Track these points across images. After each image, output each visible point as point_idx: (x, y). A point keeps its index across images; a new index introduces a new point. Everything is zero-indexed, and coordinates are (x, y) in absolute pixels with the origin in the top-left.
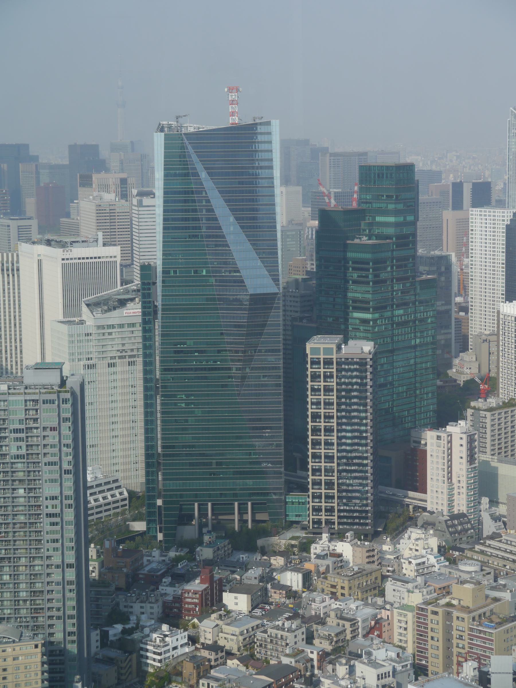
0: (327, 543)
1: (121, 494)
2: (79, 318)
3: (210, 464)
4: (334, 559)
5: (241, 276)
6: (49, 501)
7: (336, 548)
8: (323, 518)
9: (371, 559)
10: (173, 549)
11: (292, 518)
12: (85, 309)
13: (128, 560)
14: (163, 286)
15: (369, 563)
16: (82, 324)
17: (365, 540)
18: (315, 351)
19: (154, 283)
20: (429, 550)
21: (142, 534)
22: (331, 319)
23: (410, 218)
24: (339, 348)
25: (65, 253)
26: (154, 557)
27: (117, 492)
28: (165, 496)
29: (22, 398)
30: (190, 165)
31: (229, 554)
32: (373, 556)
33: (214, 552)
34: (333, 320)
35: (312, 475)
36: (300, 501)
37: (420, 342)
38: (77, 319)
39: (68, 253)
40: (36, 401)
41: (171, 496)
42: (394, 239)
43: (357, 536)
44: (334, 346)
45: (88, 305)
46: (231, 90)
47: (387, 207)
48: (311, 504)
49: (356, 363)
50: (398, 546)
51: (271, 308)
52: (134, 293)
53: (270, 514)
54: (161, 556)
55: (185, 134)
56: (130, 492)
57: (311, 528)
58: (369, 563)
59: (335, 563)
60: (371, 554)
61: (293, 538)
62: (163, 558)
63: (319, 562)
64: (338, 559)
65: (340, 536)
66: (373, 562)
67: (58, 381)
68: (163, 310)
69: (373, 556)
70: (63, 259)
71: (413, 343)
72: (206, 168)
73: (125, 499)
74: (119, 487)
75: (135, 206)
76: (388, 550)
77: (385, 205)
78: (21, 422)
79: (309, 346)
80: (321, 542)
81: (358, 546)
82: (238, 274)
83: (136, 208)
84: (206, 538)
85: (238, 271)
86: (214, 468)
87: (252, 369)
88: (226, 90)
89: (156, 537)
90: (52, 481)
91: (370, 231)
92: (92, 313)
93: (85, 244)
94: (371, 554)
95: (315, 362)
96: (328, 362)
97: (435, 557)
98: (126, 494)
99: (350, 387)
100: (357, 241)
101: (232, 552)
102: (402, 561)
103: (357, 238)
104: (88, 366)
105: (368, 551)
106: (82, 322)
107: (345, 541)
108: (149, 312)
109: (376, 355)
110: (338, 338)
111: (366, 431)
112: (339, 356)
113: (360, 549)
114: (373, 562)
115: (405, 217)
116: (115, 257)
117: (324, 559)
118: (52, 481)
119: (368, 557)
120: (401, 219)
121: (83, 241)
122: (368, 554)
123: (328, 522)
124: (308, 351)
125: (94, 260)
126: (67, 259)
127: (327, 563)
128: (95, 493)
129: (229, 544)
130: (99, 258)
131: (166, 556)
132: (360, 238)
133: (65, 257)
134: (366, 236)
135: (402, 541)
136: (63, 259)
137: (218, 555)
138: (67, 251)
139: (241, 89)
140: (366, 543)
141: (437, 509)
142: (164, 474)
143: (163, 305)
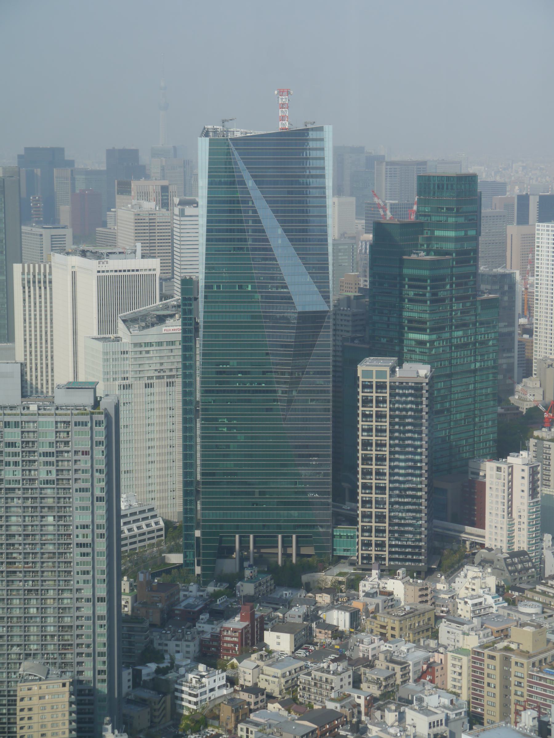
0: (377, 580)
1: (157, 523)
2: (115, 335)
3: (253, 493)
4: (384, 597)
6: (79, 529)
7: (386, 586)
8: (373, 553)
9: (424, 599)
10: (212, 583)
12: (121, 325)
14: (205, 302)
15: (421, 602)
16: (118, 341)
17: (418, 578)
18: (367, 374)
19: (196, 299)
20: (486, 590)
21: (179, 567)
23: (472, 233)
25: (101, 265)
27: (152, 522)
28: (204, 527)
29: (52, 419)
31: (271, 590)
32: (427, 595)
33: (256, 588)
34: (387, 341)
35: (362, 507)
38: (112, 336)
39: (104, 265)
40: (67, 423)
41: (210, 527)
42: (454, 255)
43: (410, 573)
44: (388, 369)
45: (124, 321)
46: (281, 92)
47: (447, 221)
49: (411, 388)
50: (453, 584)
51: (321, 327)
52: (174, 309)
53: (316, 548)
54: (199, 590)
55: (231, 139)
56: (167, 522)
58: (421, 602)
60: (424, 592)
62: (201, 593)
63: (368, 600)
64: (389, 598)
65: (391, 573)
67: (92, 402)
70: (99, 272)
71: (473, 367)
72: (253, 176)
73: (161, 530)
74: (155, 516)
75: (177, 215)
76: (442, 588)
77: (445, 218)
78: (51, 444)
80: (370, 579)
81: (411, 584)
82: (285, 290)
83: (178, 218)
84: (248, 573)
85: (286, 287)
87: (299, 392)
88: (276, 92)
90: (83, 508)
92: (129, 330)
94: (424, 592)
95: (367, 386)
96: (381, 386)
98: (162, 524)
99: (404, 413)
100: (414, 257)
101: (275, 588)
103: (414, 253)
104: (124, 386)
105: (421, 590)
109: (432, 379)
112: (394, 379)
113: (412, 587)
115: (466, 232)
116: (154, 270)
117: (373, 597)
118: (83, 508)
119: (421, 596)
120: (462, 233)
122: (420, 593)
123: (378, 558)
124: (359, 374)
126: (103, 272)
129: (271, 579)
130: (137, 270)
131: (203, 591)
132: (417, 254)
134: (424, 251)
135: (457, 579)
136: (99, 272)
137: (259, 591)
138: (103, 263)
139: (292, 92)
140: (419, 581)
142: (203, 503)
143: (204, 322)
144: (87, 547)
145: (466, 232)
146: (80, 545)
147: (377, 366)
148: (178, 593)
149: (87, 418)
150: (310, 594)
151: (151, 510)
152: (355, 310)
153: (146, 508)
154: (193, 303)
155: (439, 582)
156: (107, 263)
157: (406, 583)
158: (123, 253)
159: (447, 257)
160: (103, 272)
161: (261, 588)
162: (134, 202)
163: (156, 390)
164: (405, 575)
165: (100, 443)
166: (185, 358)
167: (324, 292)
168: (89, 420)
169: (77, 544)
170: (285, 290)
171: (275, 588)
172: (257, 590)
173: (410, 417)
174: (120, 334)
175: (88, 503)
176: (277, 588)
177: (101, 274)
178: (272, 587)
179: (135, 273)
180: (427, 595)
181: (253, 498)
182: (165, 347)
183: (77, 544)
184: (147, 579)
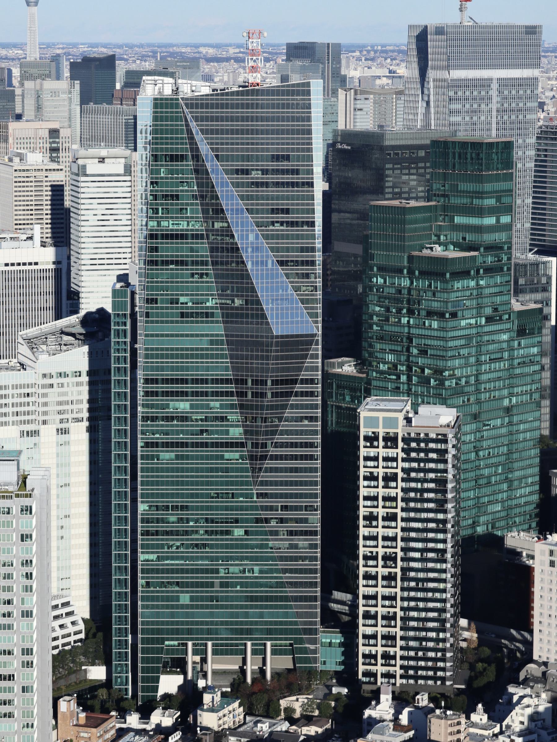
3: (212, 585)
18: (373, 422)
20: (539, 723)
23: (505, 219)
27: (67, 621)
37: (517, 402)
47: (472, 203)
51: (305, 357)
55: (182, 99)
71: (506, 402)
76: (479, 721)
77: (469, 200)
79: (364, 414)
86: (217, 592)
87: (276, 445)
96: (391, 441)
97: (549, 734)
99: (422, 475)
100: (426, 252)
103: (427, 248)
104: (28, 432)
109: (457, 425)
128: (76, 633)
129: (240, 707)
132: (431, 249)
139: (266, 34)
141: (540, 657)
145: (498, 220)
150: (294, 727)
153: (59, 602)
161: (226, 719)
165: (27, 537)
173: (432, 481)
180: (459, 732)
181: (212, 592)
184: (72, 709)
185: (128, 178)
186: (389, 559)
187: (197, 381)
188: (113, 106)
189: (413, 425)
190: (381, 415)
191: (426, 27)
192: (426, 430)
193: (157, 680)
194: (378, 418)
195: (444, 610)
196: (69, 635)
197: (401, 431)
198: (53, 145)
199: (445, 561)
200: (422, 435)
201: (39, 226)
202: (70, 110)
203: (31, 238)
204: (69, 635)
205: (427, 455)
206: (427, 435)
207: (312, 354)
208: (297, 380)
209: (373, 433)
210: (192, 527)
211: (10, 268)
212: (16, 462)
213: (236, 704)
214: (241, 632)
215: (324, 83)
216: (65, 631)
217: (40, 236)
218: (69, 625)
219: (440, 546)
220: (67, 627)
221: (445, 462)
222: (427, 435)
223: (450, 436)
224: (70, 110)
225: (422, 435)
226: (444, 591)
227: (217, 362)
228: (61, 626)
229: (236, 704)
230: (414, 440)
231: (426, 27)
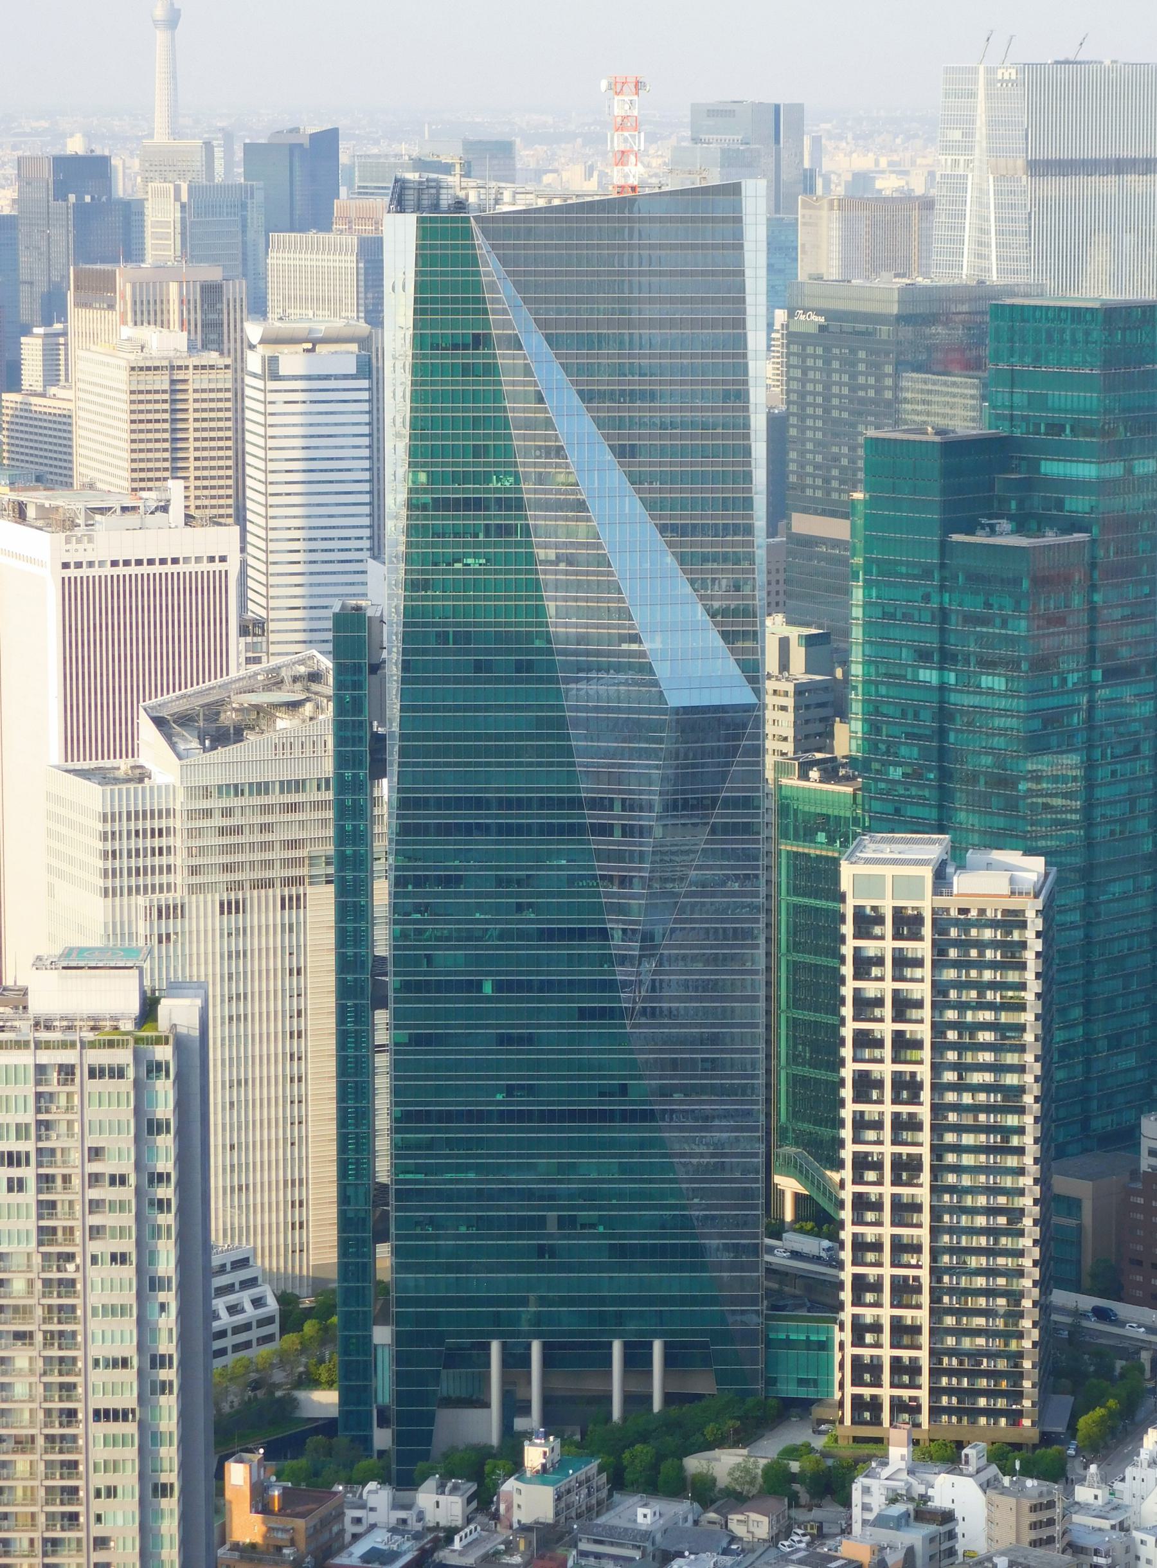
0: (904, 1476)
1: (258, 1302)
2: (131, 761)
4: (931, 1529)
5: (643, 654)
6: (100, 1370)
7: (931, 1492)
8: (886, 1392)
9: (1044, 1533)
10: (431, 1483)
11: (790, 1389)
12: (148, 732)
13: (300, 1523)
14: (404, 681)
15: (1034, 1543)
16: (141, 780)
17: (1027, 1472)
18: (872, 884)
19: (376, 668)
21: (328, 1427)
22: (900, 771)
24: (941, 879)
25: (73, 545)
26: (372, 1509)
27: (245, 1297)
28: (400, 1320)
29: (25, 1058)
30: (495, 312)
31: (599, 1503)
32: (1051, 1522)
33: (559, 1498)
34: (905, 775)
35: (854, 1263)
36: (813, 1338)
38: (123, 765)
39: (80, 547)
40: (67, 1071)
41: (419, 1319)
42: (1095, 530)
43: (1002, 1456)
44: (927, 873)
45: (160, 722)
46: (617, 87)
48: (850, 1351)
49: (994, 924)
50: (1118, 1485)
52: (298, 686)
53: (721, 1378)
54: (396, 1506)
56: (285, 1299)
57: (848, 1421)
58: (1034, 1543)
59: (932, 1540)
60: (1044, 1516)
61: (792, 1452)
62: (402, 1514)
63: (885, 1536)
64: (943, 1529)
65: (950, 1456)
66: (1050, 1540)
67: (134, 1007)
68: (403, 752)
69: (1051, 1522)
70: (66, 566)
72: (541, 324)
73: (269, 1320)
74: (252, 1283)
75: (255, 375)
76: (1091, 1500)
78: (21, 1131)
80: (886, 1472)
81: (1004, 1491)
82: (634, 647)
83: (259, 384)
84: (534, 1455)
85: (635, 639)
88: (604, 84)
89: (367, 1441)
90: (112, 1311)
91: (1021, 503)
92: (173, 746)
93: (131, 519)
94: (1044, 1516)
95: (866, 923)
98: (272, 1305)
101: (610, 1495)
102: (1137, 1535)
105: (1034, 1509)
106: (140, 776)
107: (961, 1474)
108: (358, 754)
110: (933, 848)
111: (1021, 1131)
112: (942, 901)
113: (1011, 1501)
114: (1050, 1540)
115: (1129, 471)
116: (223, 559)
117: (898, 1527)
118: (112, 1311)
119: (1034, 1526)
120: (1115, 470)
121: (124, 509)
122: (1034, 1517)
123: (899, 1406)
124: (846, 885)
125: (157, 569)
126: (79, 565)
127: (907, 1543)
129: (600, 1471)
130: (175, 561)
131: (407, 1507)
133: (71, 559)
134: (1010, 518)
135: (1129, 1471)
136: (66, 566)
137: (568, 1507)
138: (79, 541)
140: (1030, 1483)
142: (397, 1252)
143: (403, 737)
144: (125, 1419)
146: (102, 1415)
147: (895, 862)
148: (341, 1515)
149: (123, 1056)
151: (243, 1263)
152: (805, 678)
154: (369, 680)
155: (1082, 1480)
156: (90, 541)
157: (986, 1486)
158: (134, 508)
159: (1078, 536)
160: (79, 565)
162: (127, 331)
163: (253, 918)
164: (984, 1461)
166: (342, 837)
167: (744, 651)
168: (131, 1060)
169: (97, 1412)
170: (634, 647)
171: (610, 1495)
172: (563, 1505)
174: (144, 759)
175: (129, 1297)
176: (617, 1496)
177: (72, 572)
178: (604, 1494)
179: (169, 568)
182: (275, 798)
183: (97, 1412)
185: (365, 383)
186: (906, 1169)
187: (508, 804)
188: (332, 235)
189: (955, 891)
190: (889, 871)
191: (327, 141)
192: (981, 903)
193: (430, 1419)
194: (882, 877)
195: (1020, 1273)
196: (237, 1348)
197: (926, 904)
198: (211, 316)
199: (1021, 1111)
200: (973, 914)
201: (181, 483)
202: (244, 243)
203: (165, 509)
204: (247, 1327)
205: (981, 994)
206: (982, 912)
207: (726, 799)
208: (737, 747)
209: (874, 908)
210: (500, 1103)
211: (121, 570)
212: (136, 972)
213: (595, 1464)
214: (602, 1318)
215: (346, 377)
216: (239, 1319)
217: (183, 503)
218: (248, 1306)
219: (1011, 1079)
220: (243, 1311)
221: (1022, 966)
222: (982, 912)
223: (1030, 915)
224: (244, 243)
225: (973, 914)
226: (1021, 1171)
227: (551, 764)
228: (233, 1310)
229: (595, 1464)
230: (956, 923)
231: (327, 141)
